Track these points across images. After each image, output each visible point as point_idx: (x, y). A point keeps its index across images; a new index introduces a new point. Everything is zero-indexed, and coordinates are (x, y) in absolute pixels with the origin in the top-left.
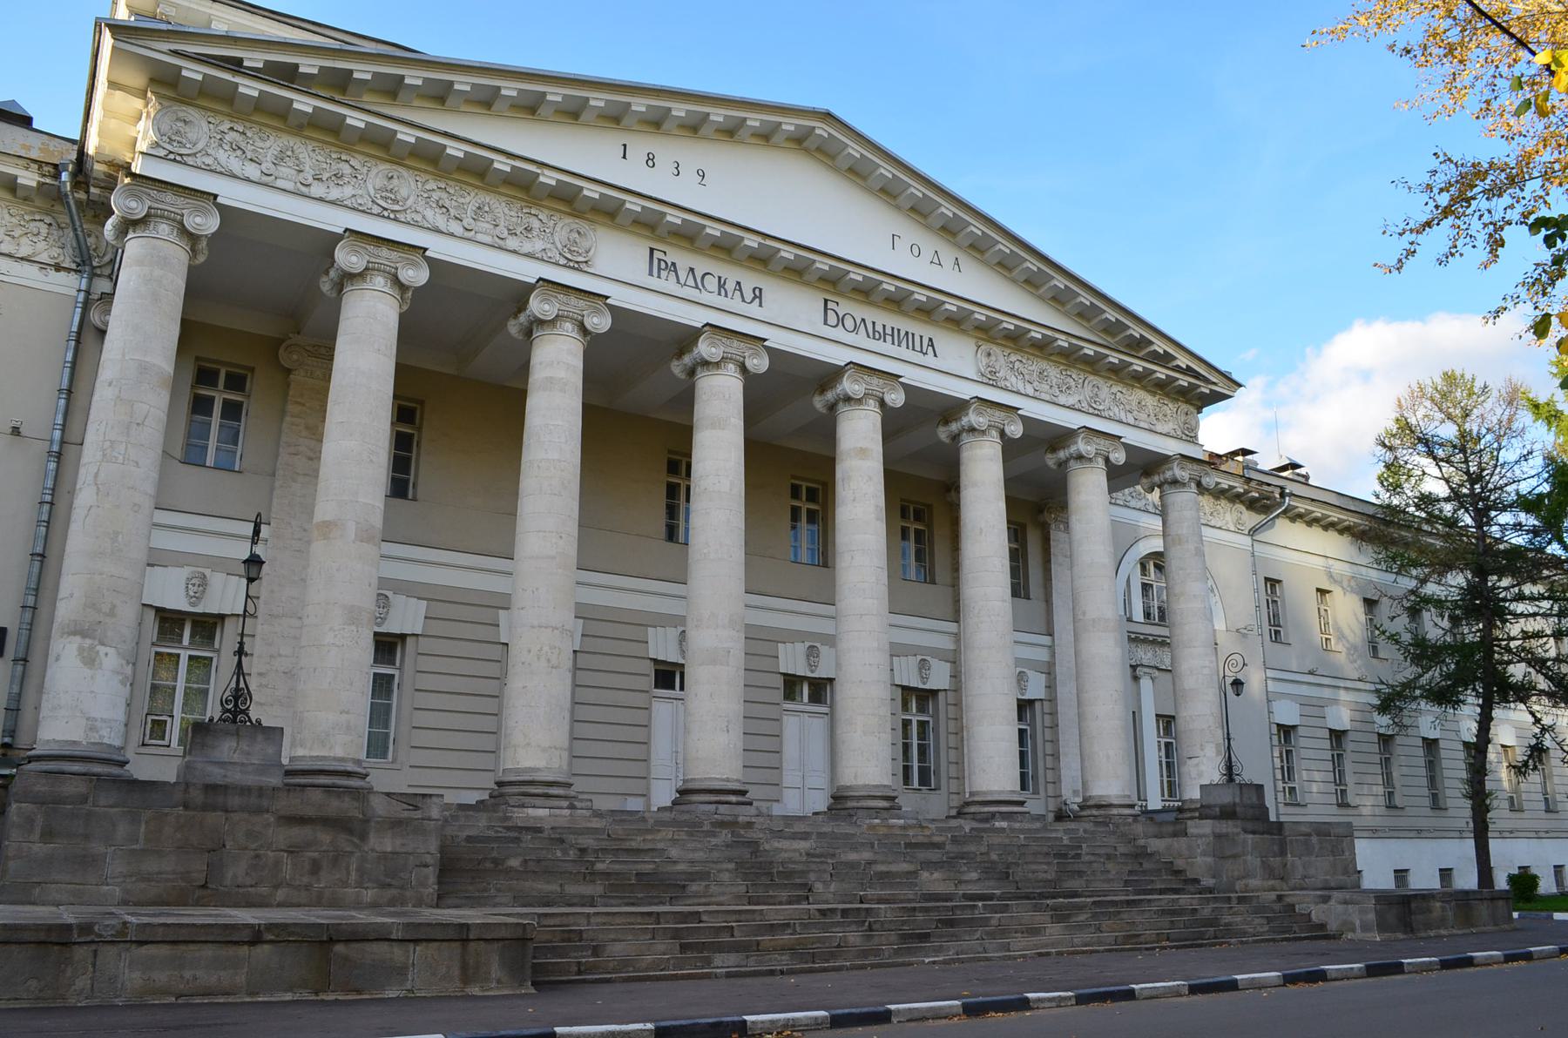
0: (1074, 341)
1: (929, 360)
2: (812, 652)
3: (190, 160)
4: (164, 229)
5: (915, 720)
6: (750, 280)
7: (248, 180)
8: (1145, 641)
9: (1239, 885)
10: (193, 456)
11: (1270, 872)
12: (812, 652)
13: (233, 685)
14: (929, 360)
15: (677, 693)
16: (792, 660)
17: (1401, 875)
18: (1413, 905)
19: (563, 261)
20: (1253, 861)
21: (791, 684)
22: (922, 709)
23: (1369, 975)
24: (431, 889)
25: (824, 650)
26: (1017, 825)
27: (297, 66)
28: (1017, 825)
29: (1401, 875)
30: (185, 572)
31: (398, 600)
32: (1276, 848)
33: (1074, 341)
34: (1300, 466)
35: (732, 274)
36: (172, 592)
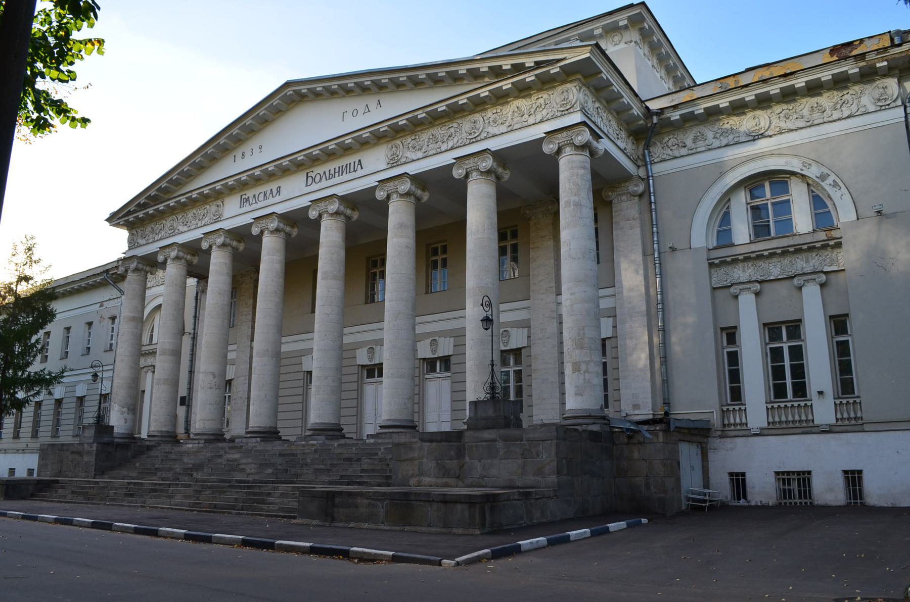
0: (429, 109)
1: (360, 172)
2: (434, 343)
3: (479, 138)
4: (568, 150)
5: (511, 371)
6: (273, 186)
7: (419, 159)
8: (772, 255)
9: (413, 481)
10: (428, 289)
11: (445, 472)
12: (434, 343)
13: (490, 381)
14: (360, 172)
15: (376, 379)
16: (363, 358)
17: (12, 471)
18: (337, 500)
19: (559, 114)
20: (430, 464)
21: (430, 364)
22: (518, 362)
23: (92, 527)
24: (93, 473)
25: (377, 349)
26: (380, 441)
27: (501, 66)
28: (380, 441)
29: (12, 471)
30: (428, 341)
31: (441, 341)
32: (452, 453)
33: (429, 109)
34: (31, 278)
35: (266, 188)
36: (424, 351)
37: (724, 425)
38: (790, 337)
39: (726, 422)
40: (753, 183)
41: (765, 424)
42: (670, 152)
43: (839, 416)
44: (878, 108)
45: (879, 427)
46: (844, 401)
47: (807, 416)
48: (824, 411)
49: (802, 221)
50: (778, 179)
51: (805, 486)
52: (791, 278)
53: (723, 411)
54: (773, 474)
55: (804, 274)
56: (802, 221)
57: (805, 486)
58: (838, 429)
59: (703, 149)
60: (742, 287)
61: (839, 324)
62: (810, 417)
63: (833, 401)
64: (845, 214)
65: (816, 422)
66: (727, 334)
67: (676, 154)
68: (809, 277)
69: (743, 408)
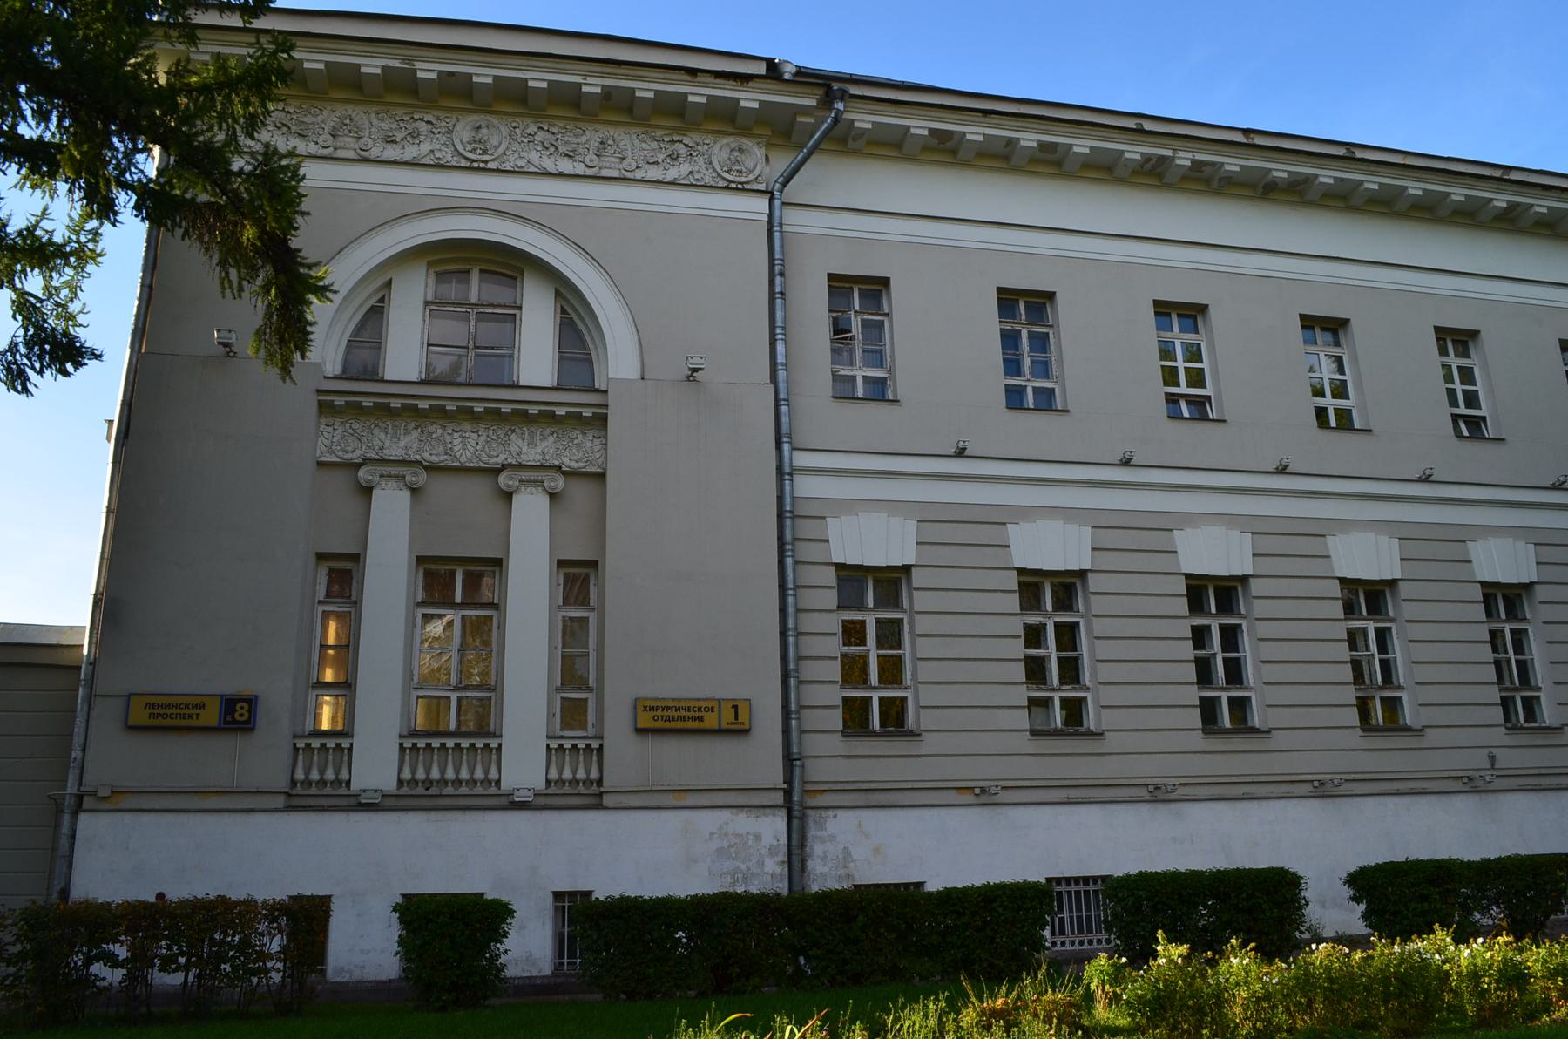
37: (294, 783)
38: (880, 603)
39: (300, 775)
40: (453, 259)
41: (390, 784)
42: (534, 157)
43: (407, 775)
44: (722, 183)
45: (213, 802)
46: (567, 744)
47: (486, 772)
48: (523, 761)
49: (536, 358)
50: (508, 264)
51: (1080, 918)
52: (496, 471)
53: (296, 749)
54: (550, 898)
55: (520, 466)
56: (536, 358)
57: (1080, 918)
58: (550, 801)
59: (351, 154)
60: (525, 475)
61: (577, 578)
62: (493, 774)
63: (398, 741)
64: (619, 360)
65: (355, 786)
66: (331, 571)
67: (374, 153)
68: (533, 475)
69: (345, 744)
